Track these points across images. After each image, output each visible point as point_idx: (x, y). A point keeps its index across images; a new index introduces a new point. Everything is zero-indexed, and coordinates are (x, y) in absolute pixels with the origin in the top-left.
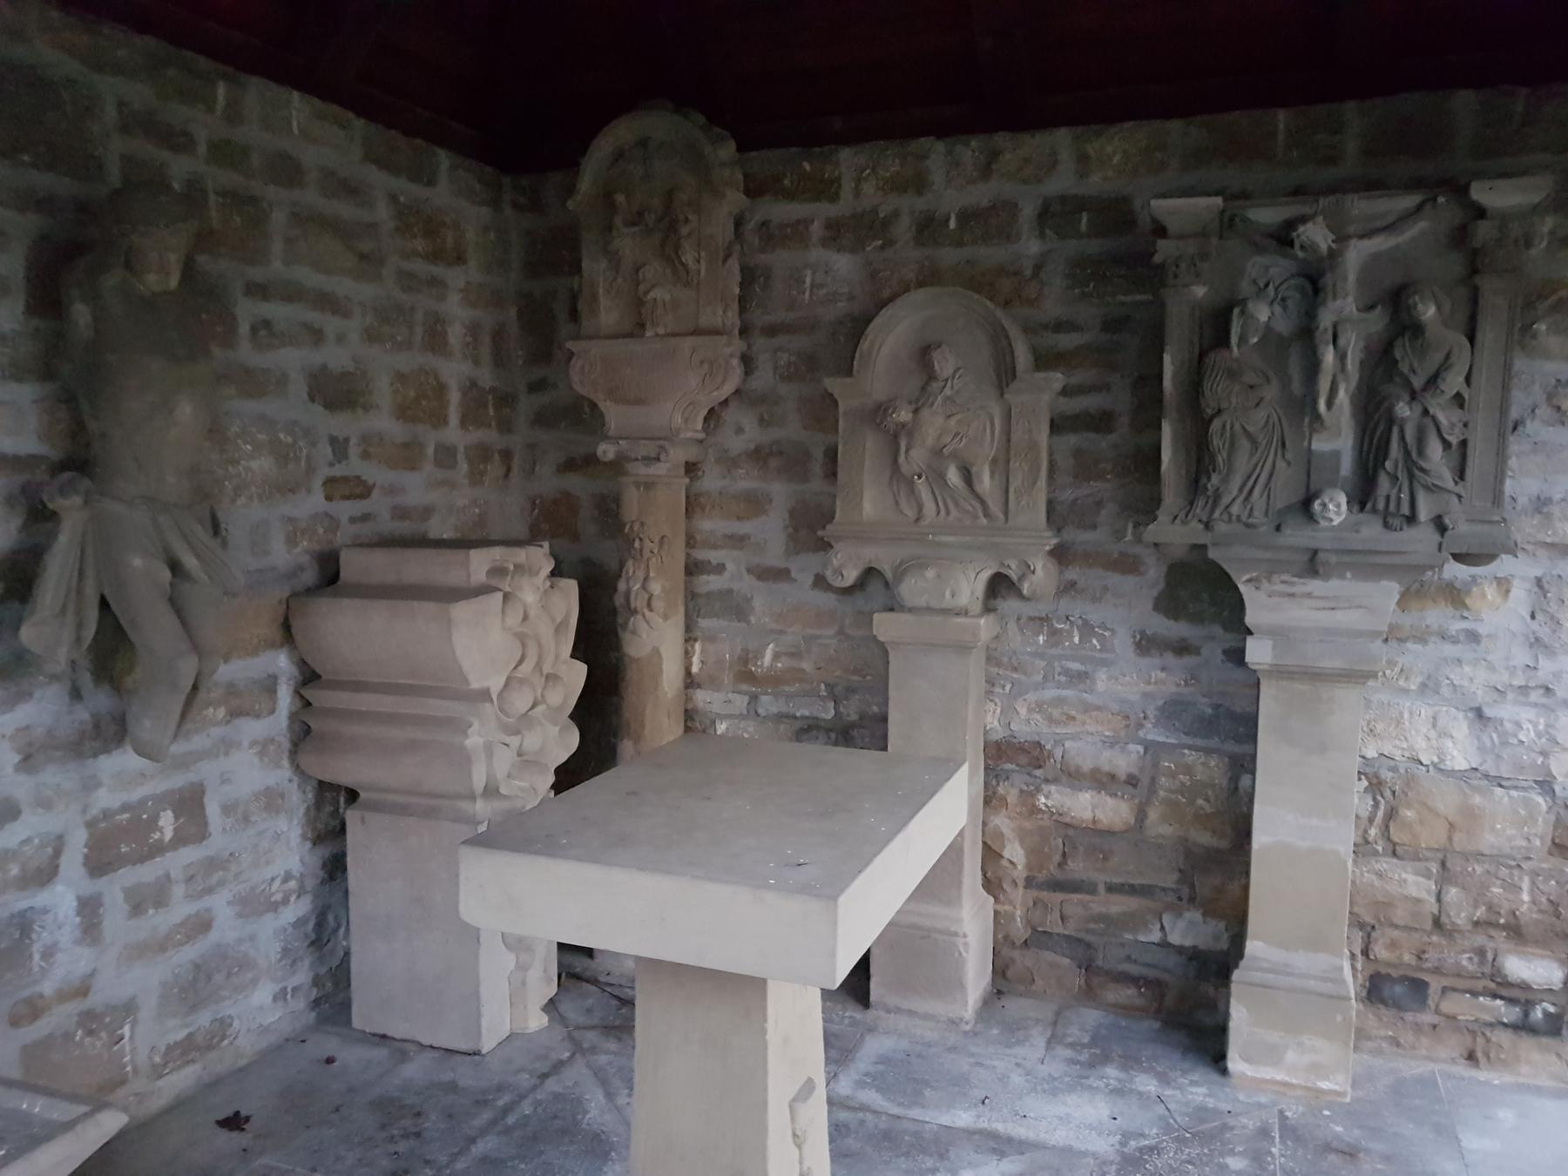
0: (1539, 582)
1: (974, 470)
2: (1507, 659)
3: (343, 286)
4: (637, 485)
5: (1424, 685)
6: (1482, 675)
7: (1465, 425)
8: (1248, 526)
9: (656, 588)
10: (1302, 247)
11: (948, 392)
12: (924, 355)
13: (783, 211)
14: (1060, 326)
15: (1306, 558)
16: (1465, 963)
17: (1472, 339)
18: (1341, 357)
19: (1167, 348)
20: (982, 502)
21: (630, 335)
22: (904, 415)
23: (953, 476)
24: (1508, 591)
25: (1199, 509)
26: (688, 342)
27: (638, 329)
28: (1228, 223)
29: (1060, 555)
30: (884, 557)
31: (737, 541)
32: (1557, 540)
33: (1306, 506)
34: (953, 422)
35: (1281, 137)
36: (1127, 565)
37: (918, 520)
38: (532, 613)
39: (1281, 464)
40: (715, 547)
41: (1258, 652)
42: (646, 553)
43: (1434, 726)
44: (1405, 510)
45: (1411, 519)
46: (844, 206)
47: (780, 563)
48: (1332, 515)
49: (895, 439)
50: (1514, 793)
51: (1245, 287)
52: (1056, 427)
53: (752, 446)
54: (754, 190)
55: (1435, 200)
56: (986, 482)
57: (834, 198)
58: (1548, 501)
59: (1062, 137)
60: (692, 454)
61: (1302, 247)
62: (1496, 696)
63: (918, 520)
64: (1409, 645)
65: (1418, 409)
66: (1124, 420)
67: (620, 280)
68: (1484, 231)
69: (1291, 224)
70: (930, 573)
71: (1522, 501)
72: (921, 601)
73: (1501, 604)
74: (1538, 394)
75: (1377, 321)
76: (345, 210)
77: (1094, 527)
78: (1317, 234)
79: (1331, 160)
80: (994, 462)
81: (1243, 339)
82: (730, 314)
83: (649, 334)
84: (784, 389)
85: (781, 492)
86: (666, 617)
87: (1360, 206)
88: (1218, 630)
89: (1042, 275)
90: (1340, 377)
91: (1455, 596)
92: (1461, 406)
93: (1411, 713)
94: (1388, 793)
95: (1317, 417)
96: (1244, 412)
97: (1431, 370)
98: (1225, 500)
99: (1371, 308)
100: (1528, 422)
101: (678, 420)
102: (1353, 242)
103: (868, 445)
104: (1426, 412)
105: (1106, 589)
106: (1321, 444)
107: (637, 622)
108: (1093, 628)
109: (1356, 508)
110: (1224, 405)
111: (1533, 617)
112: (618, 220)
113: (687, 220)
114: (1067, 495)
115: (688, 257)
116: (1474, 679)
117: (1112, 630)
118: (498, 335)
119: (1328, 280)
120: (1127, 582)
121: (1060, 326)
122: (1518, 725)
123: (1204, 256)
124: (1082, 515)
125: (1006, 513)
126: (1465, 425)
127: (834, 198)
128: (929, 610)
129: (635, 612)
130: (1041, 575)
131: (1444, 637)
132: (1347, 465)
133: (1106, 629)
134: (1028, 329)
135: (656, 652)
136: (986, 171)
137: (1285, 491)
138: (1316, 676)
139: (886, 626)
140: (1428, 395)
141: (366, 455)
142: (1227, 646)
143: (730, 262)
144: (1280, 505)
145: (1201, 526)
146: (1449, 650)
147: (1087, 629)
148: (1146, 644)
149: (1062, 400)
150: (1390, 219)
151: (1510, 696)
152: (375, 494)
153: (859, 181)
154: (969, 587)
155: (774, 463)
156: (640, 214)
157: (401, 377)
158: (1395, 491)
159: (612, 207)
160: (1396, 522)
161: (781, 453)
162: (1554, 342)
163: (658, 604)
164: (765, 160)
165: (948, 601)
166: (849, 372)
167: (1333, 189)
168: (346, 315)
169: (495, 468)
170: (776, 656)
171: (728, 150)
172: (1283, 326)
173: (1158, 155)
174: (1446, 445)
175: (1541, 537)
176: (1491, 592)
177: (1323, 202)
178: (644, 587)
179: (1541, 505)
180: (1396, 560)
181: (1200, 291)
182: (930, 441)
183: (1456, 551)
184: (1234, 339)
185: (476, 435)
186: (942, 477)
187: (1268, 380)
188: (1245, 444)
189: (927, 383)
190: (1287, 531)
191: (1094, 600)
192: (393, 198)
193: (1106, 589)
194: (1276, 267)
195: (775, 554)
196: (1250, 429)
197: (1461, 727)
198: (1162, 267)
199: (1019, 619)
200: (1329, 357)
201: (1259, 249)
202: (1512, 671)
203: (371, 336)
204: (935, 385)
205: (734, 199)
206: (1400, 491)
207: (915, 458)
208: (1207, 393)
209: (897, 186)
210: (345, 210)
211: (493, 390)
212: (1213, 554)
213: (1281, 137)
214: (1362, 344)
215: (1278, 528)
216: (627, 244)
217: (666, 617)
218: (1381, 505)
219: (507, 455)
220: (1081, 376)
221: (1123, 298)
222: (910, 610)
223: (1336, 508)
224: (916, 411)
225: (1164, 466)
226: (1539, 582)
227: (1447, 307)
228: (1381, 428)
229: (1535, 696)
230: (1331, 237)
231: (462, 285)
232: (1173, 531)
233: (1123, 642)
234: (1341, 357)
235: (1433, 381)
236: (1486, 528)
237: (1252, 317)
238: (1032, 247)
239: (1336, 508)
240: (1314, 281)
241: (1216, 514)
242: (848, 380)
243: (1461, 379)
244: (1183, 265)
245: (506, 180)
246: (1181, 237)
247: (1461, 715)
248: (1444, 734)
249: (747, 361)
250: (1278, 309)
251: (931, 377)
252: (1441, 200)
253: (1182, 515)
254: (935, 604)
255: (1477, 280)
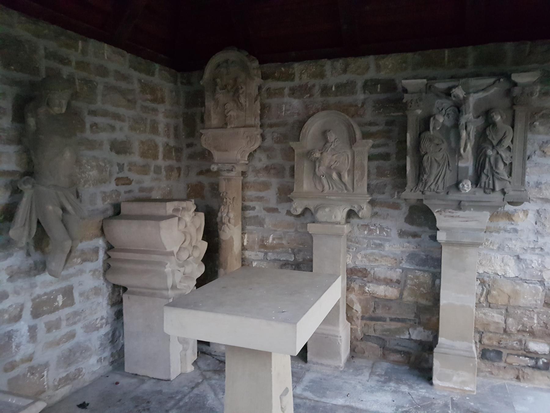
0: (538, 211)
1: (342, 174)
2: (527, 238)
3: (122, 111)
4: (225, 179)
5: (499, 248)
6: (519, 244)
7: (511, 157)
8: (437, 192)
9: (232, 215)
10: (454, 96)
11: (332, 146)
12: (324, 134)
13: (273, 84)
14: (371, 124)
15: (457, 203)
16: (515, 345)
17: (513, 127)
18: (468, 134)
19: (408, 131)
20: (345, 185)
21: (222, 128)
22: (317, 155)
23: (335, 176)
24: (527, 215)
25: (420, 187)
26: (242, 130)
27: (224, 125)
28: (429, 88)
29: (372, 203)
30: (306, 203)
31: (260, 199)
32: (544, 197)
33: (457, 186)
34: (334, 157)
35: (446, 59)
36: (395, 206)
37: (323, 191)
38: (188, 224)
39: (448, 171)
40: (252, 201)
41: (441, 236)
42: (228, 203)
43: (503, 262)
44: (491, 187)
45: (493, 190)
46: (297, 82)
47: (275, 207)
48: (466, 189)
49: (314, 163)
50: (531, 285)
51: (435, 110)
52: (370, 159)
53: (265, 166)
54: (265, 77)
55: (499, 80)
56: (346, 178)
57: (293, 80)
58: (541, 183)
59: (371, 58)
60: (243, 169)
61: (454, 96)
62: (524, 251)
63: (323, 191)
64: (494, 234)
65: (495, 152)
66: (394, 156)
67: (218, 108)
68: (516, 91)
69: (450, 88)
70: (327, 210)
71: (532, 183)
72: (324, 220)
73: (525, 219)
74: (536, 146)
75: (480, 122)
76: (123, 85)
77: (384, 193)
78: (459, 92)
79: (464, 66)
80: (349, 171)
81: (434, 128)
82: (257, 120)
83: (229, 127)
84: (276, 146)
85: (275, 182)
86: (235, 226)
87: (474, 82)
88: (427, 229)
89: (365, 106)
90: (468, 141)
91: (509, 216)
92: (510, 151)
93: (494, 257)
94: (487, 285)
95: (460, 155)
96: (436, 154)
97: (500, 139)
98: (429, 184)
99: (478, 117)
100: (533, 156)
101: (239, 157)
102: (472, 95)
103: (305, 165)
104: (498, 153)
105: (388, 214)
106: (461, 164)
107: (225, 227)
108: (384, 228)
109: (474, 186)
110: (428, 151)
111: (536, 224)
112: (218, 88)
113: (242, 88)
114: (374, 182)
115: (242, 100)
116: (516, 246)
117: (390, 229)
118: (176, 128)
119: (463, 108)
120: (396, 212)
121: (371, 124)
122: (532, 261)
123: (421, 100)
124: (380, 189)
125: (353, 188)
126: (511, 157)
127: (293, 80)
128: (326, 222)
129: (224, 224)
130: (366, 210)
131: (506, 231)
132: (471, 171)
133: (388, 229)
134: (360, 125)
135: (232, 238)
136: (345, 71)
137: (450, 179)
138: (461, 244)
139: (312, 228)
140: (498, 147)
141: (130, 170)
142: (430, 234)
143: (256, 102)
144: (448, 185)
145: (421, 193)
146: (507, 235)
147: (382, 229)
148: (402, 234)
149: (372, 149)
150: (485, 87)
151: (529, 251)
152: (133, 183)
153: (301, 74)
154: (341, 214)
155: (272, 171)
156: (226, 86)
157: (142, 143)
158: (487, 181)
159: (216, 84)
160: (488, 191)
161: (275, 168)
162: (541, 129)
163: (232, 221)
164: (269, 67)
165: (333, 219)
166: (298, 140)
167: (466, 76)
168: (123, 121)
169: (175, 174)
170: (273, 239)
171: (256, 64)
172: (448, 124)
173: (404, 65)
174: (505, 164)
175: (538, 196)
176: (521, 215)
177: (462, 81)
178: (227, 215)
179: (538, 185)
180: (488, 204)
181: (419, 112)
182: (326, 164)
183: (509, 201)
184: (431, 128)
185: (169, 162)
186: (331, 176)
187: (443, 142)
188: (435, 165)
189: (325, 144)
190: (450, 194)
191: (384, 219)
192: (140, 81)
193: (388, 214)
194: (446, 103)
195: (273, 204)
196: (437, 159)
197: (512, 262)
198: (406, 104)
199: (358, 225)
200: (464, 134)
201: (438, 96)
202: (529, 242)
203: (132, 128)
204: (328, 144)
205: (258, 81)
206: (489, 180)
207: (322, 170)
208: (422, 146)
209: (314, 76)
210: (123, 85)
211: (173, 147)
212: (425, 202)
213: (446, 59)
214: (475, 130)
215: (448, 193)
216: (221, 96)
217: (235, 226)
218: (483, 185)
219: (179, 169)
220: (378, 141)
221: (393, 114)
222: (320, 222)
223: (467, 186)
224: (322, 153)
225: (407, 173)
226: (538, 211)
227: (505, 117)
228: (482, 159)
229: (537, 251)
230: (464, 93)
231: (163, 110)
232: (411, 194)
233: (394, 233)
234: (468, 134)
235: (500, 142)
236: (519, 193)
237: (437, 120)
238: (361, 96)
239: (467, 186)
240: (458, 108)
241: (426, 189)
242: (298, 143)
243: (510, 141)
244: (413, 103)
245: (179, 74)
246: (412, 93)
247: (512, 258)
248: (506, 265)
249: (263, 137)
250: (446, 117)
251: (327, 141)
252: (502, 80)
253: (414, 189)
254: (328, 221)
255: (515, 107)
